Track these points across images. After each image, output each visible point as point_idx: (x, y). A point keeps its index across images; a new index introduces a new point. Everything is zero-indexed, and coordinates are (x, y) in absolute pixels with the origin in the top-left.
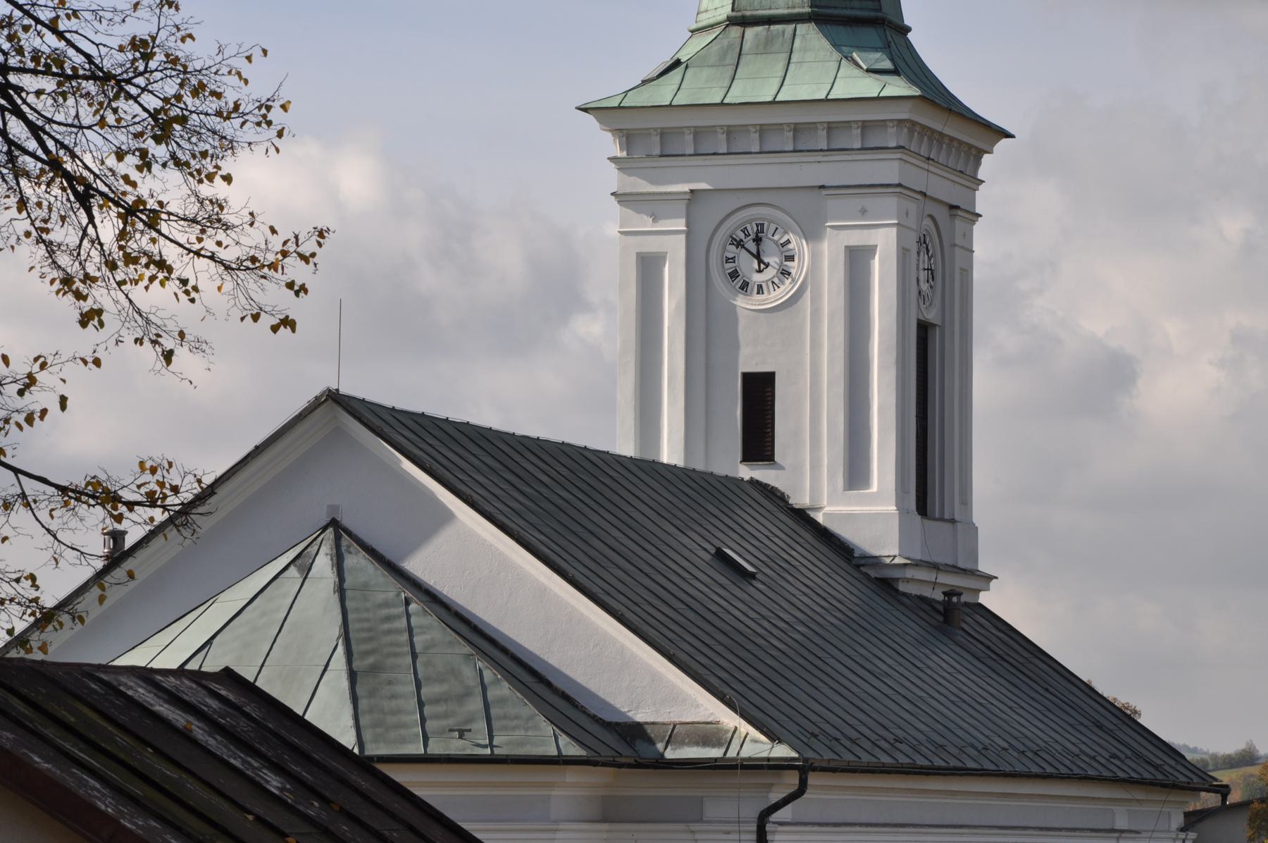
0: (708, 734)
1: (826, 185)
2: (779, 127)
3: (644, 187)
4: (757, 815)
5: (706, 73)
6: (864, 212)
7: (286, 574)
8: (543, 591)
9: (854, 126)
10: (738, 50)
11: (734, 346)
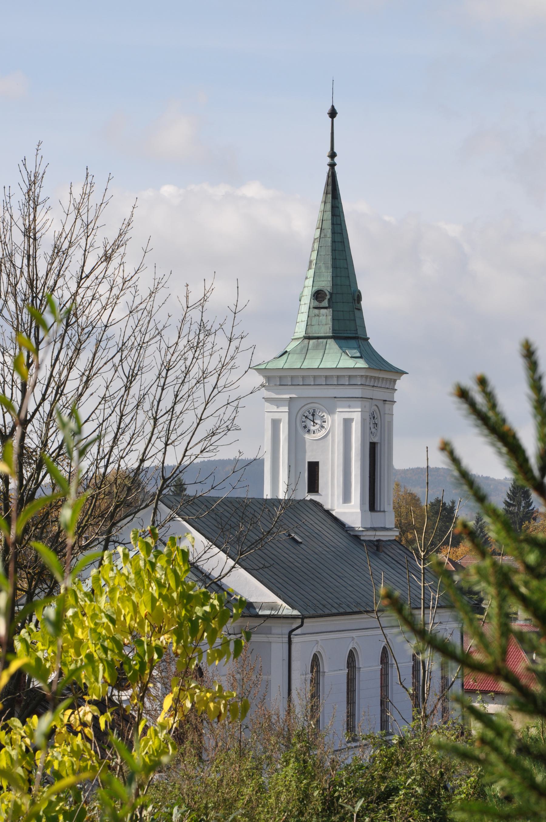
0: (273, 606)
3: (274, 396)
5: (296, 356)
6: (349, 407)
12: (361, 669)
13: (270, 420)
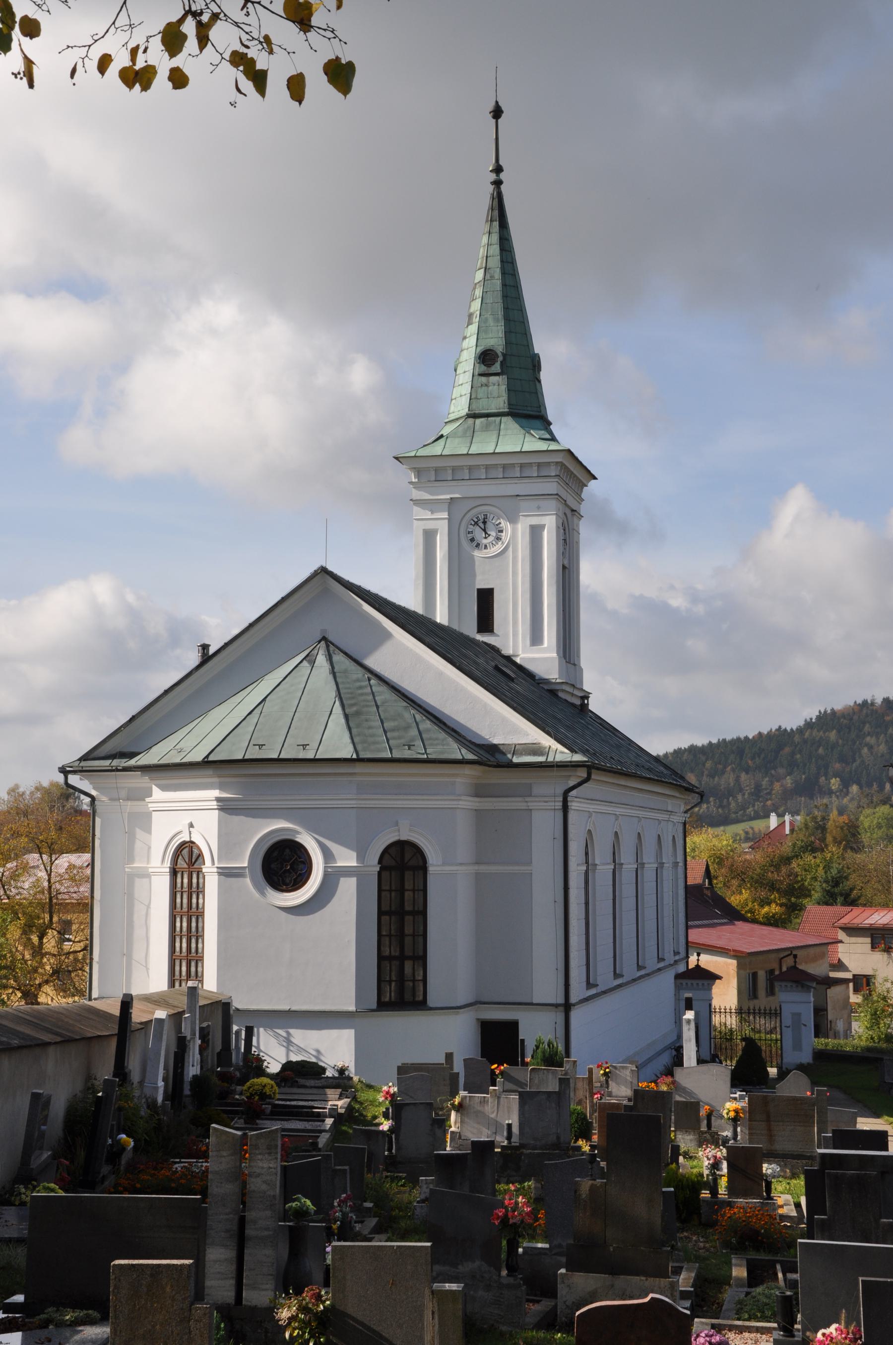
0: (536, 749)
2: (495, 466)
3: (427, 496)
4: (562, 792)
5: (457, 440)
6: (539, 508)
7: (301, 665)
8: (441, 674)
9: (533, 465)
11: (474, 575)
12: (624, 866)
13: (422, 531)
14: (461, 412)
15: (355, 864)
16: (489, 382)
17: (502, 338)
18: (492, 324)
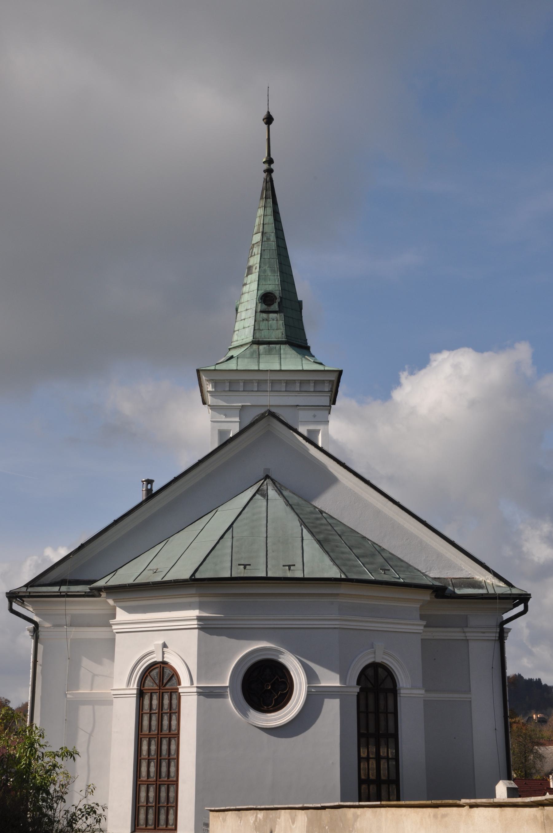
1: (299, 405)
2: (280, 381)
5: (246, 360)
7: (255, 497)
9: (311, 381)
10: (258, 353)
14: (244, 341)
15: (338, 685)
16: (269, 318)
17: (278, 285)
18: (270, 274)
